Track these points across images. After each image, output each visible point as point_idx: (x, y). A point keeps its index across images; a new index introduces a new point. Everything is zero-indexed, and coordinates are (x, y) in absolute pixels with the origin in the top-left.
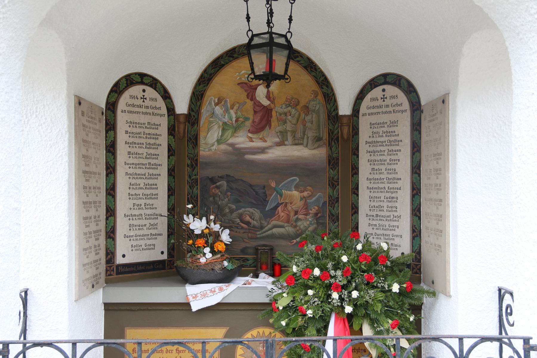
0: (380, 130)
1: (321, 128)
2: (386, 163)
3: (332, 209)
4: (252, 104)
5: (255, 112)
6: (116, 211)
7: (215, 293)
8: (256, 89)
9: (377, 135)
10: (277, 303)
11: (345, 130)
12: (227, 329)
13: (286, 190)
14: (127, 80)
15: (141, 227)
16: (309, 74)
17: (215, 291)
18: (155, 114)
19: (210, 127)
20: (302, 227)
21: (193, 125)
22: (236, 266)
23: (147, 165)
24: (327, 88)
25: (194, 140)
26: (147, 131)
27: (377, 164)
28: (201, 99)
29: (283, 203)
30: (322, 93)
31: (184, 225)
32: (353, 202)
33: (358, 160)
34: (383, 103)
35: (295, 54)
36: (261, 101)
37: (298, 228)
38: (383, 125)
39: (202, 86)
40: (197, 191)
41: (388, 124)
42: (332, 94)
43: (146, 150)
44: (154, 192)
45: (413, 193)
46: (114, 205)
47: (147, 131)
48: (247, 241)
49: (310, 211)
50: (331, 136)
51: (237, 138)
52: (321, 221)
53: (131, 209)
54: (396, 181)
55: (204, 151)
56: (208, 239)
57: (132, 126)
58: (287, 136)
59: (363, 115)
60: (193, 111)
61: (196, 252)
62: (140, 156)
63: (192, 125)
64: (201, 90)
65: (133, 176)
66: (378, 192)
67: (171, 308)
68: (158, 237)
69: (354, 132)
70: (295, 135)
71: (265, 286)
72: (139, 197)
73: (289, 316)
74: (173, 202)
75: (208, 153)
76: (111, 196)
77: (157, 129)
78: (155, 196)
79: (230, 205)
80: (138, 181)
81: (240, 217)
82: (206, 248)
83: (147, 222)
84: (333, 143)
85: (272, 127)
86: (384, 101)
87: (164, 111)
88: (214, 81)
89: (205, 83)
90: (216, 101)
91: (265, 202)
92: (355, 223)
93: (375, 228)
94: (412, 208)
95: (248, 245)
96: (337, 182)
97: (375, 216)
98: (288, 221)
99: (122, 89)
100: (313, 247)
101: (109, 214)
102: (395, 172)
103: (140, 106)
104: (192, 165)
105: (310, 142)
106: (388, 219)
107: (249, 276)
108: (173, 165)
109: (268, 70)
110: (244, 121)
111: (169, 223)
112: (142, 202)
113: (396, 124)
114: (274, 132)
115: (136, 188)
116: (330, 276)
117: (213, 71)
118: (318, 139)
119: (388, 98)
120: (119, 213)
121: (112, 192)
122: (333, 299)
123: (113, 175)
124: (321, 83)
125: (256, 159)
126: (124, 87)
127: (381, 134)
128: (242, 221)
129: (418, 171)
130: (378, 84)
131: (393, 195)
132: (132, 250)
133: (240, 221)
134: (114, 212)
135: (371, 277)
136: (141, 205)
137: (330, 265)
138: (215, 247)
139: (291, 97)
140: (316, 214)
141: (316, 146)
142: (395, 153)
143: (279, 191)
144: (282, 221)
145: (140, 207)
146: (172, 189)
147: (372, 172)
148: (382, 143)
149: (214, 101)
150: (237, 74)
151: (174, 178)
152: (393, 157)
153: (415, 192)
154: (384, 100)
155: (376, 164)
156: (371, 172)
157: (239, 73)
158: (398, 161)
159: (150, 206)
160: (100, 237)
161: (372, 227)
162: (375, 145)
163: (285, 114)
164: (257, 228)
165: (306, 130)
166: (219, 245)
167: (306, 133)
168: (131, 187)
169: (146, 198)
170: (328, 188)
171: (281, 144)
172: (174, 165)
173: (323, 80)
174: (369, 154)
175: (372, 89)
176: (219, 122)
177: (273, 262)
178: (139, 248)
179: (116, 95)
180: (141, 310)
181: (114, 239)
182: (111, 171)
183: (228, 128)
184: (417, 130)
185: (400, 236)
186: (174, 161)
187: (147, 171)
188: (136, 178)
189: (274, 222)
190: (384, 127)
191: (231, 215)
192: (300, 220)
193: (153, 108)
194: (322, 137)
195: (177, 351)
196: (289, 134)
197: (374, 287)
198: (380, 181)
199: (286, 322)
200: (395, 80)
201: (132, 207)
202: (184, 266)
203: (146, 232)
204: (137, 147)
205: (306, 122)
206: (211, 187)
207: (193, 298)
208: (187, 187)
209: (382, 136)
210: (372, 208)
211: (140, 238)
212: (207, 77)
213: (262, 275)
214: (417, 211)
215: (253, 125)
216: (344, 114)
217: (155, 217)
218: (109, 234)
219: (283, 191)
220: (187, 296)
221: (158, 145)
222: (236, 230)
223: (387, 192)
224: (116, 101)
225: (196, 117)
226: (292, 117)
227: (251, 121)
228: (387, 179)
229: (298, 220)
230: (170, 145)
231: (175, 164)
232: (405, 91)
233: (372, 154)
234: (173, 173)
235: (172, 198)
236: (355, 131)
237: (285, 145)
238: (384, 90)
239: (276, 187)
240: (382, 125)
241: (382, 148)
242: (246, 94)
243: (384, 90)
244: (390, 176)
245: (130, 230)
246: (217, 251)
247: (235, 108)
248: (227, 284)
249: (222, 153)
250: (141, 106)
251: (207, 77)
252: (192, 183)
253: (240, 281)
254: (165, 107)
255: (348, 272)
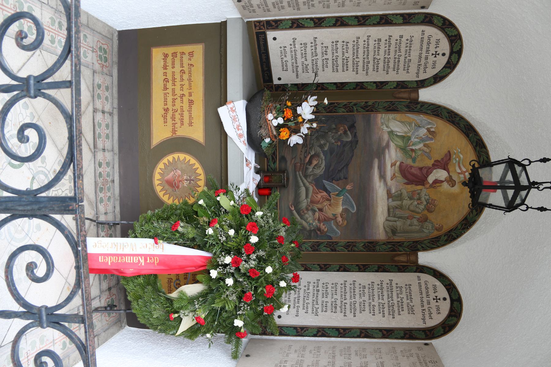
0: (404, 295)
1: (405, 235)
2: (371, 301)
3: (325, 245)
4: (429, 165)
5: (421, 169)
6: (320, 28)
7: (237, 130)
8: (444, 169)
9: (399, 292)
10: (224, 194)
11: (403, 259)
12: (203, 144)
13: (343, 200)
14: (455, 36)
15: (304, 55)
16: (459, 223)
17: (238, 129)
18: (420, 67)
19: (406, 123)
20: (307, 215)
21: (408, 106)
22: (265, 151)
23: (367, 60)
24: (444, 240)
25: (393, 108)
26: (402, 59)
27: (369, 292)
28: (433, 114)
29: (331, 198)
30: (440, 235)
31: (306, 96)
32: (332, 266)
33: (373, 272)
34: (431, 299)
35: (480, 208)
36: (432, 174)
37: (306, 212)
38: (409, 298)
39: (447, 115)
40: (342, 112)
41: (411, 303)
42: (439, 245)
43: (382, 58)
44: (340, 68)
45: (341, 329)
46: (326, 26)
47: (402, 59)
48: (293, 162)
49: (322, 224)
50: (397, 244)
51: (394, 150)
52: (312, 234)
53: (322, 44)
54: (353, 311)
55: (382, 118)
56: (293, 121)
57: (407, 42)
58: (398, 200)
59: (418, 277)
60: (421, 106)
61: (279, 110)
62: (377, 52)
63: (407, 106)
64: (443, 114)
65: (356, 46)
66: (342, 292)
67: (222, 87)
68: (295, 74)
69: (401, 267)
70: (399, 208)
71: (245, 181)
72: (335, 52)
73: (211, 207)
74: (330, 88)
75: (380, 122)
76: (335, 22)
77: (404, 70)
78: (335, 69)
79: (328, 145)
80: (350, 51)
81: (316, 155)
82: (283, 120)
83: (309, 62)
84: (390, 246)
85: (407, 186)
86: (434, 299)
87: (422, 77)
88: (452, 127)
89: (449, 118)
90: (432, 130)
91: (331, 179)
92: (310, 267)
93: (306, 288)
94: (326, 328)
95: (288, 163)
96: (351, 249)
97: (318, 288)
98: (312, 202)
99: (446, 31)
100: (283, 234)
101: (317, 21)
102: (362, 310)
103: (428, 51)
104: (367, 107)
105: (391, 223)
106: (315, 302)
107: (257, 165)
108: (367, 87)
109: (484, 184)
110: (412, 158)
111: (309, 85)
112: (329, 56)
113: (411, 313)
114: (401, 187)
115: (343, 49)
116: (249, 255)
117: (462, 126)
118: (394, 231)
119: (437, 304)
120: (318, 31)
121: (339, 23)
122: (225, 257)
123: (357, 24)
124: (449, 234)
125: (374, 170)
126: (448, 33)
127: (400, 296)
128: (312, 157)
129: (363, 335)
130: (450, 292)
131: (338, 308)
132: (281, 47)
133: (312, 155)
134: (319, 26)
135: (249, 299)
136: (326, 54)
137: (261, 253)
138: (283, 129)
139: (437, 204)
140: (319, 229)
141: (387, 229)
142: (381, 310)
143: (342, 193)
144: (312, 196)
145: (324, 54)
146: (344, 87)
147: (361, 286)
148: (391, 297)
149: (432, 127)
150: (459, 150)
151: (354, 89)
152: (376, 308)
153: (342, 331)
154: (435, 299)
155: (369, 290)
156: (362, 285)
157: (460, 152)
158: (373, 314)
159: (325, 64)
160: (292, 8)
161: (307, 286)
162: (389, 289)
163: (419, 199)
164: (305, 172)
165: (403, 219)
166: (286, 133)
167: (400, 219)
168: (345, 44)
169: (333, 59)
170: (345, 241)
171: (389, 194)
172: (367, 88)
173: (453, 236)
174: (379, 283)
175: (445, 286)
176: (411, 133)
177: (272, 187)
178: (283, 54)
179: (440, 25)
180: (221, 57)
181: (291, 28)
182: (361, 21)
183: (405, 142)
184: (405, 334)
185: (297, 314)
186: (371, 88)
187: (361, 60)
188: (354, 49)
189: (311, 189)
190: (408, 299)
191: (318, 146)
192: (314, 214)
193: (425, 64)
194: (396, 235)
195: (182, 95)
196: (399, 203)
197: (240, 298)
198: (352, 294)
199: (202, 205)
200: (456, 311)
201: (324, 45)
202: (264, 98)
203: (300, 60)
204: (385, 49)
205: (411, 220)
206: (345, 126)
207: (231, 108)
208: (345, 102)
209: (398, 297)
210: (326, 285)
211: (294, 55)
212: (455, 120)
213: (258, 178)
214: (322, 333)
215: (408, 167)
216: (419, 257)
217: (315, 69)
218: (296, 22)
219: (343, 197)
220: (233, 102)
221: (387, 71)
222: (303, 151)
223: (342, 301)
224: (434, 24)
225: (416, 110)
226: (416, 206)
227: (412, 164)
228: (355, 302)
229: (314, 211)
230: (387, 84)
231: (368, 89)
232: (445, 322)
233: (380, 286)
234: (359, 87)
235: (334, 87)
236: (402, 269)
237: (388, 199)
238: (445, 299)
239: (346, 190)
240: (409, 297)
241: (385, 297)
242: (439, 159)
243: (445, 299)
244: (357, 305)
245: (301, 44)
246: (280, 131)
247: (425, 149)
248: (246, 142)
249: (380, 136)
250: (428, 52)
251: (455, 120)
252: (349, 106)
253: (251, 156)
254: (426, 78)
255: (253, 274)
